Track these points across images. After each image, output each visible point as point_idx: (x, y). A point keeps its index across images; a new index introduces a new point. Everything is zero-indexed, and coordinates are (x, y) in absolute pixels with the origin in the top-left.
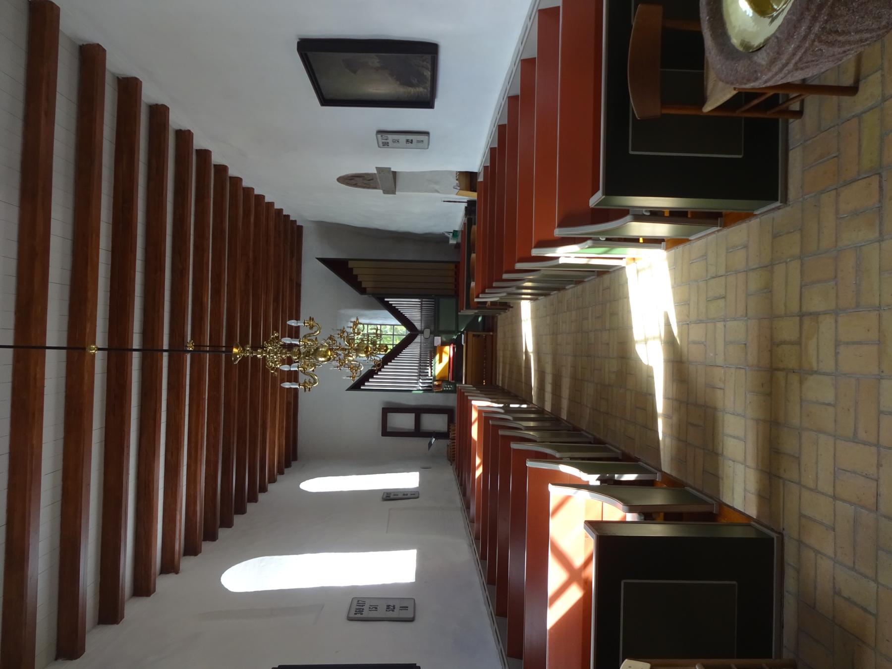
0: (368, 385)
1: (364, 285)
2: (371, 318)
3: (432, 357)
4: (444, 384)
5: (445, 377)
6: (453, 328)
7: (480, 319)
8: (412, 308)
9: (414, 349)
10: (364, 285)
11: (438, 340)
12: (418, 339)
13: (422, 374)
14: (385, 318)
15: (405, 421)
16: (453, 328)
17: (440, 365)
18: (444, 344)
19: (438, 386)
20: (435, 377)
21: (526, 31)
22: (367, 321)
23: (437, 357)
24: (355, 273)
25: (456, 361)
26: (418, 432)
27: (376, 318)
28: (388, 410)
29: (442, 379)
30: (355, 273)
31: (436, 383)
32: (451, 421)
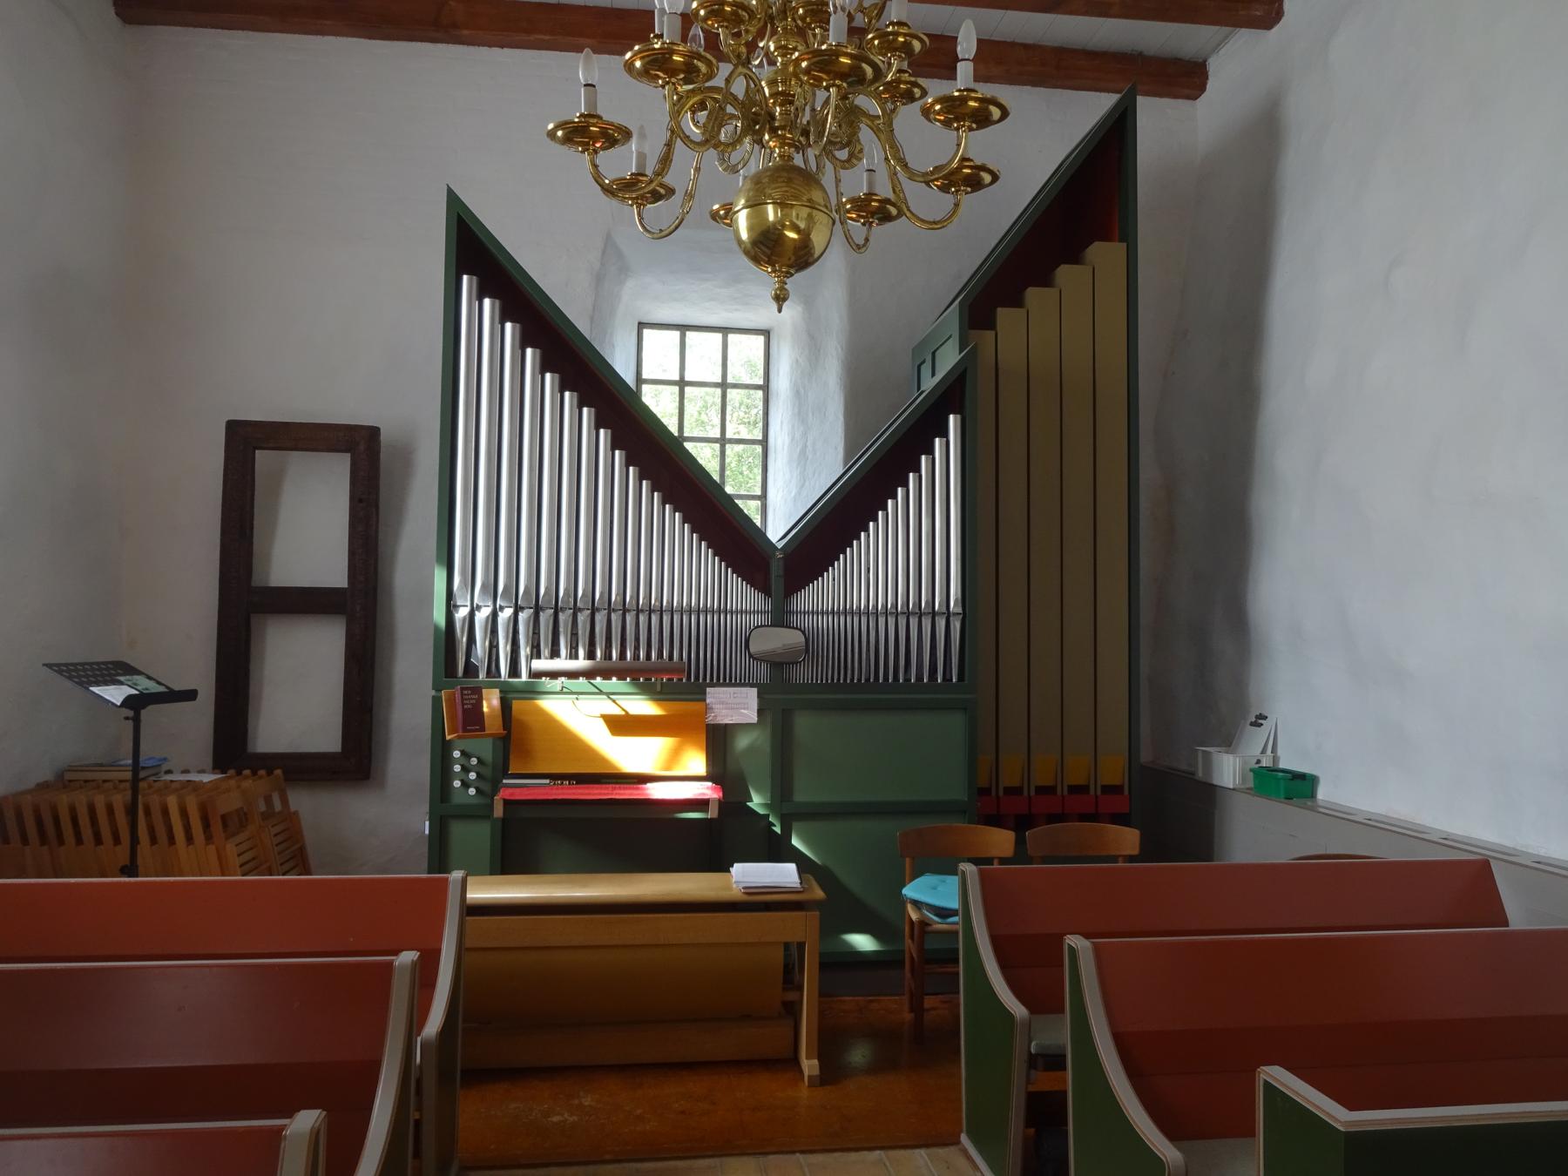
0: (482, 315)
1: (1004, 315)
2: (798, 394)
3: (643, 677)
4: (484, 748)
5: (526, 753)
6: (803, 794)
7: (862, 942)
8: (910, 560)
9: (685, 571)
10: (1004, 315)
11: (736, 706)
12: (742, 595)
13: (552, 619)
14: (802, 457)
15: (308, 538)
16: (803, 794)
17: (591, 719)
18: (718, 740)
19: (472, 718)
20: (531, 692)
21: (1447, 842)
22: (782, 382)
23: (643, 707)
24: (1033, 294)
25: (618, 825)
26: (248, 603)
27: (801, 413)
28: (362, 448)
29: (514, 736)
30: (1033, 294)
31: (491, 702)
32: (303, 769)
